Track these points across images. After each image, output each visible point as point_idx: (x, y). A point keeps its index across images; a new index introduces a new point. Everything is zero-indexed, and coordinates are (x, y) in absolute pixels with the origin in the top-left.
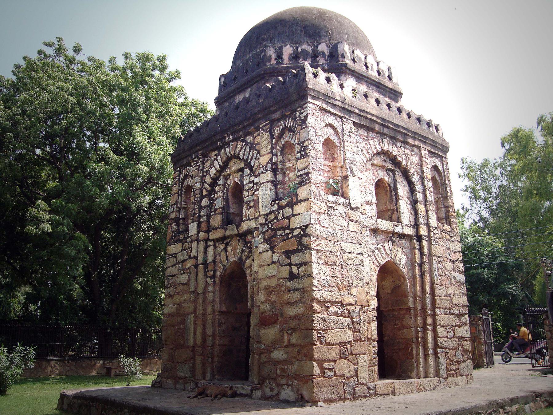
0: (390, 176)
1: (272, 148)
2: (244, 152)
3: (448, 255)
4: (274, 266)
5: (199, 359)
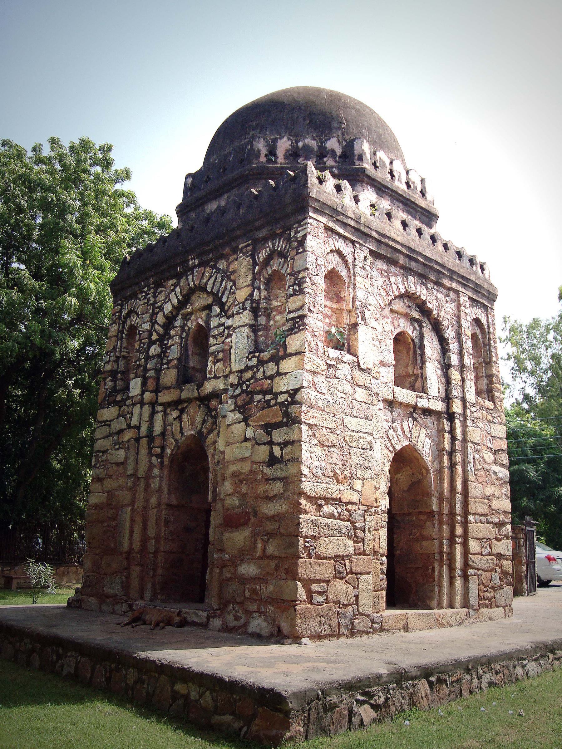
0: (414, 327)
1: (254, 279)
2: (214, 282)
3: (488, 442)
4: (248, 444)
5: (135, 571)
